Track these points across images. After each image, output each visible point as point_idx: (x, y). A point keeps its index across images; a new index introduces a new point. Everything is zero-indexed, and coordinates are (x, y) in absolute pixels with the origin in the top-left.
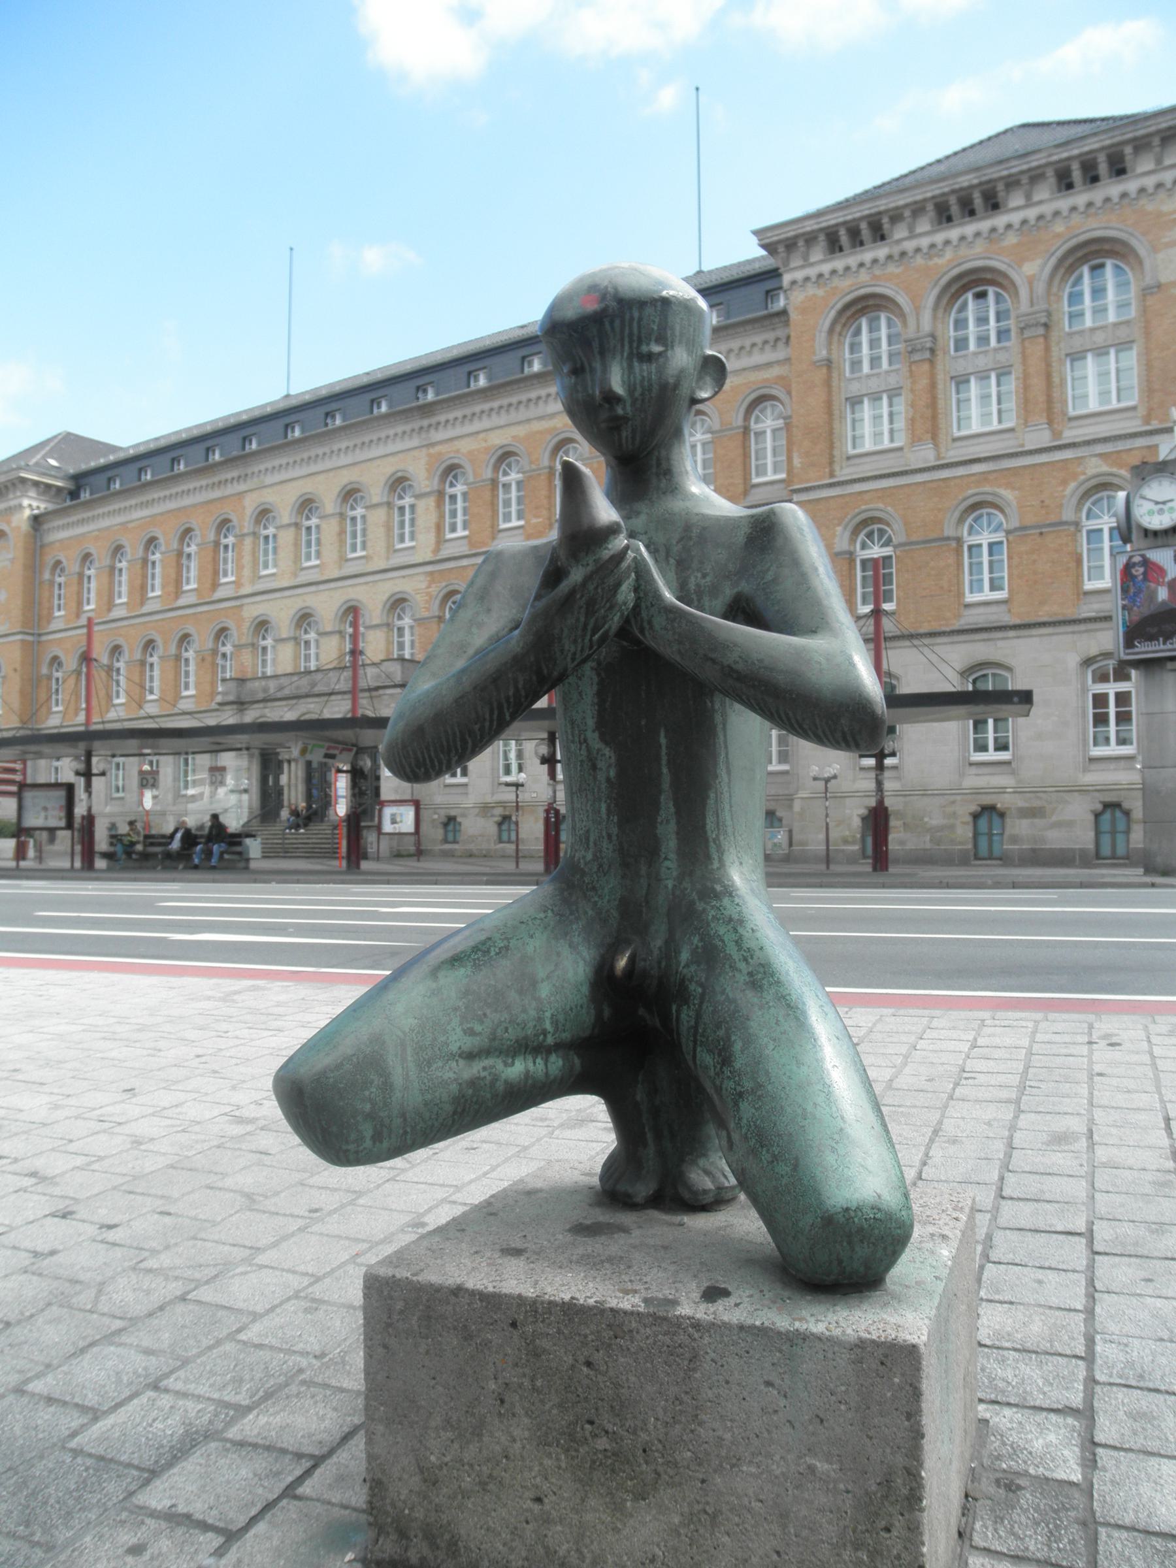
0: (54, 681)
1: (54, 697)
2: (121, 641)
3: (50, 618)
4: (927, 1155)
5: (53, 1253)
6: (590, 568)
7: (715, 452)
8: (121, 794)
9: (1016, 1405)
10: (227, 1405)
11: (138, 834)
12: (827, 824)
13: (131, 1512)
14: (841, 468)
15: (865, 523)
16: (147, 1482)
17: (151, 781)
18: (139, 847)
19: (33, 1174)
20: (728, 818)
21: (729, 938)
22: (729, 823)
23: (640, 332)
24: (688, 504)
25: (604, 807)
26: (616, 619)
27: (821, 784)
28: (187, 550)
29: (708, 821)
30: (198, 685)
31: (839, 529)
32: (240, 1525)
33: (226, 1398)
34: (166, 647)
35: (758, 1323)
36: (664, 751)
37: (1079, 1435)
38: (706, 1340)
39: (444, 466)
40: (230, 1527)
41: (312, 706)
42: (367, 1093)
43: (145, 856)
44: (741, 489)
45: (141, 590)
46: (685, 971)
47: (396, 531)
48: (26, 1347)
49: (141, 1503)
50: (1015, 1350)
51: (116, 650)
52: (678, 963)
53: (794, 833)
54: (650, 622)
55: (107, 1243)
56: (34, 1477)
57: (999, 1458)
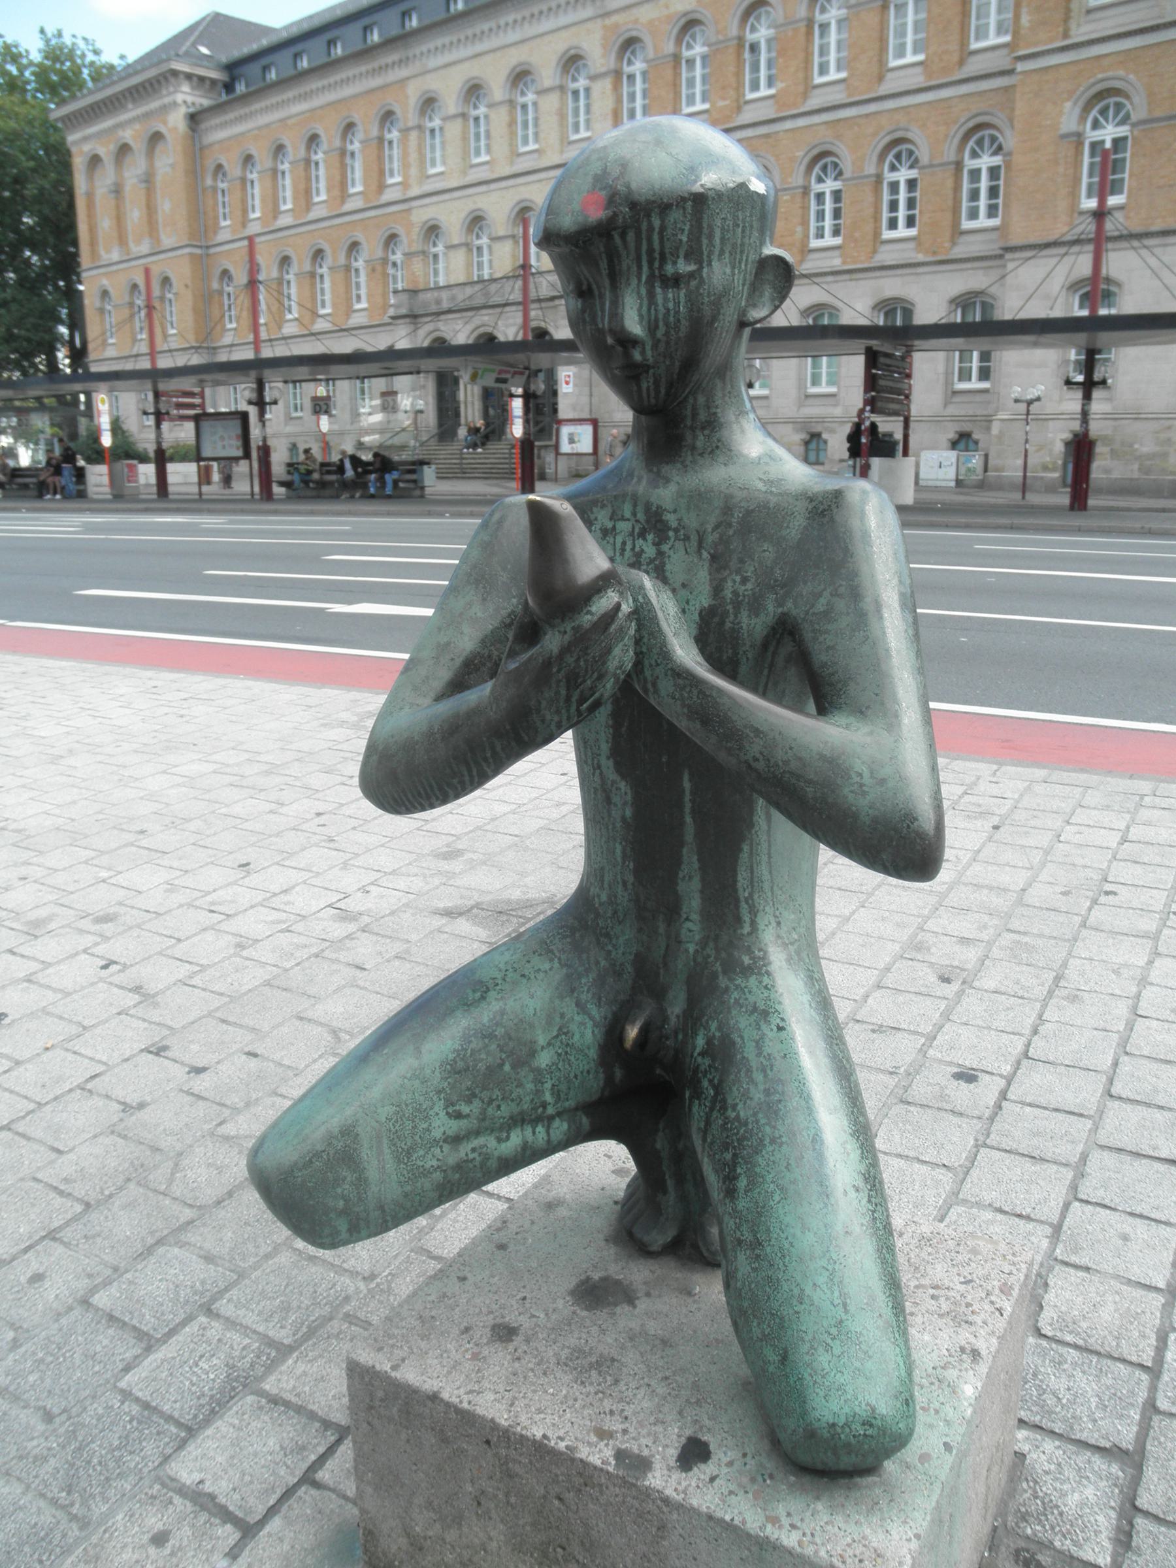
0: (226, 297)
1: (227, 314)
2: (290, 252)
3: (216, 228)
4: (1040, 1016)
5: (142, 1106)
6: (567, 638)
7: (929, 12)
8: (299, 414)
9: (1060, 1436)
10: (270, 1343)
11: (314, 461)
12: (1026, 451)
13: (164, 1485)
14: (1079, 25)
15: (1101, 95)
16: (182, 1444)
17: (324, 407)
18: (316, 476)
19: (137, 989)
20: (765, 873)
21: (749, 1034)
22: (766, 876)
24: (732, 471)
26: (609, 686)
27: (1023, 406)
28: (350, 147)
29: (740, 878)
30: (370, 296)
31: (1068, 105)
32: (258, 1517)
33: (271, 1333)
34: (335, 257)
35: (728, 1518)
36: (687, 797)
37: (1121, 1492)
38: (675, 1516)
39: (621, 40)
40: (248, 1519)
41: (486, 318)
42: (339, 1190)
43: (322, 485)
44: (955, 58)
45: (305, 195)
47: (570, 120)
48: (99, 1240)
49: (172, 1474)
50: (1076, 1347)
51: (285, 261)
52: (694, 1048)
53: (990, 457)
54: (654, 684)
55: (192, 1094)
56: (83, 1425)
57: (1024, 1517)
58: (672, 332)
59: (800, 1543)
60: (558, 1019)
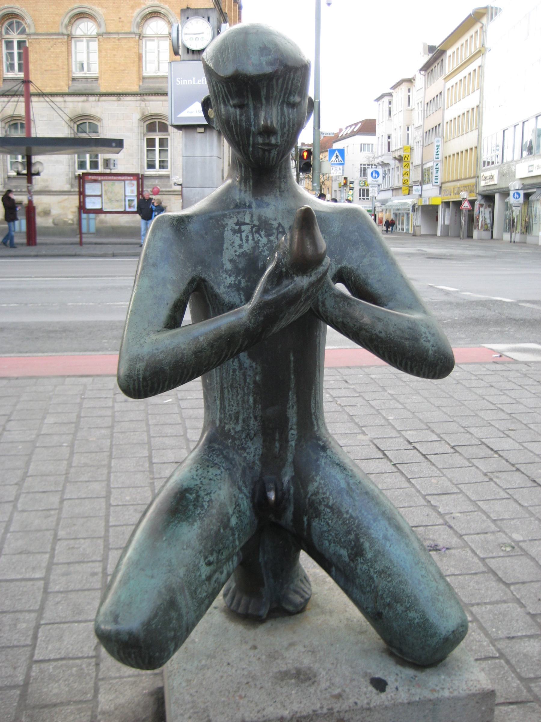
23: (291, 88)
25: (251, 400)
42: (171, 625)
46: (313, 497)
54: (323, 303)
58: (291, 130)
59: (451, 693)
60: (234, 499)
